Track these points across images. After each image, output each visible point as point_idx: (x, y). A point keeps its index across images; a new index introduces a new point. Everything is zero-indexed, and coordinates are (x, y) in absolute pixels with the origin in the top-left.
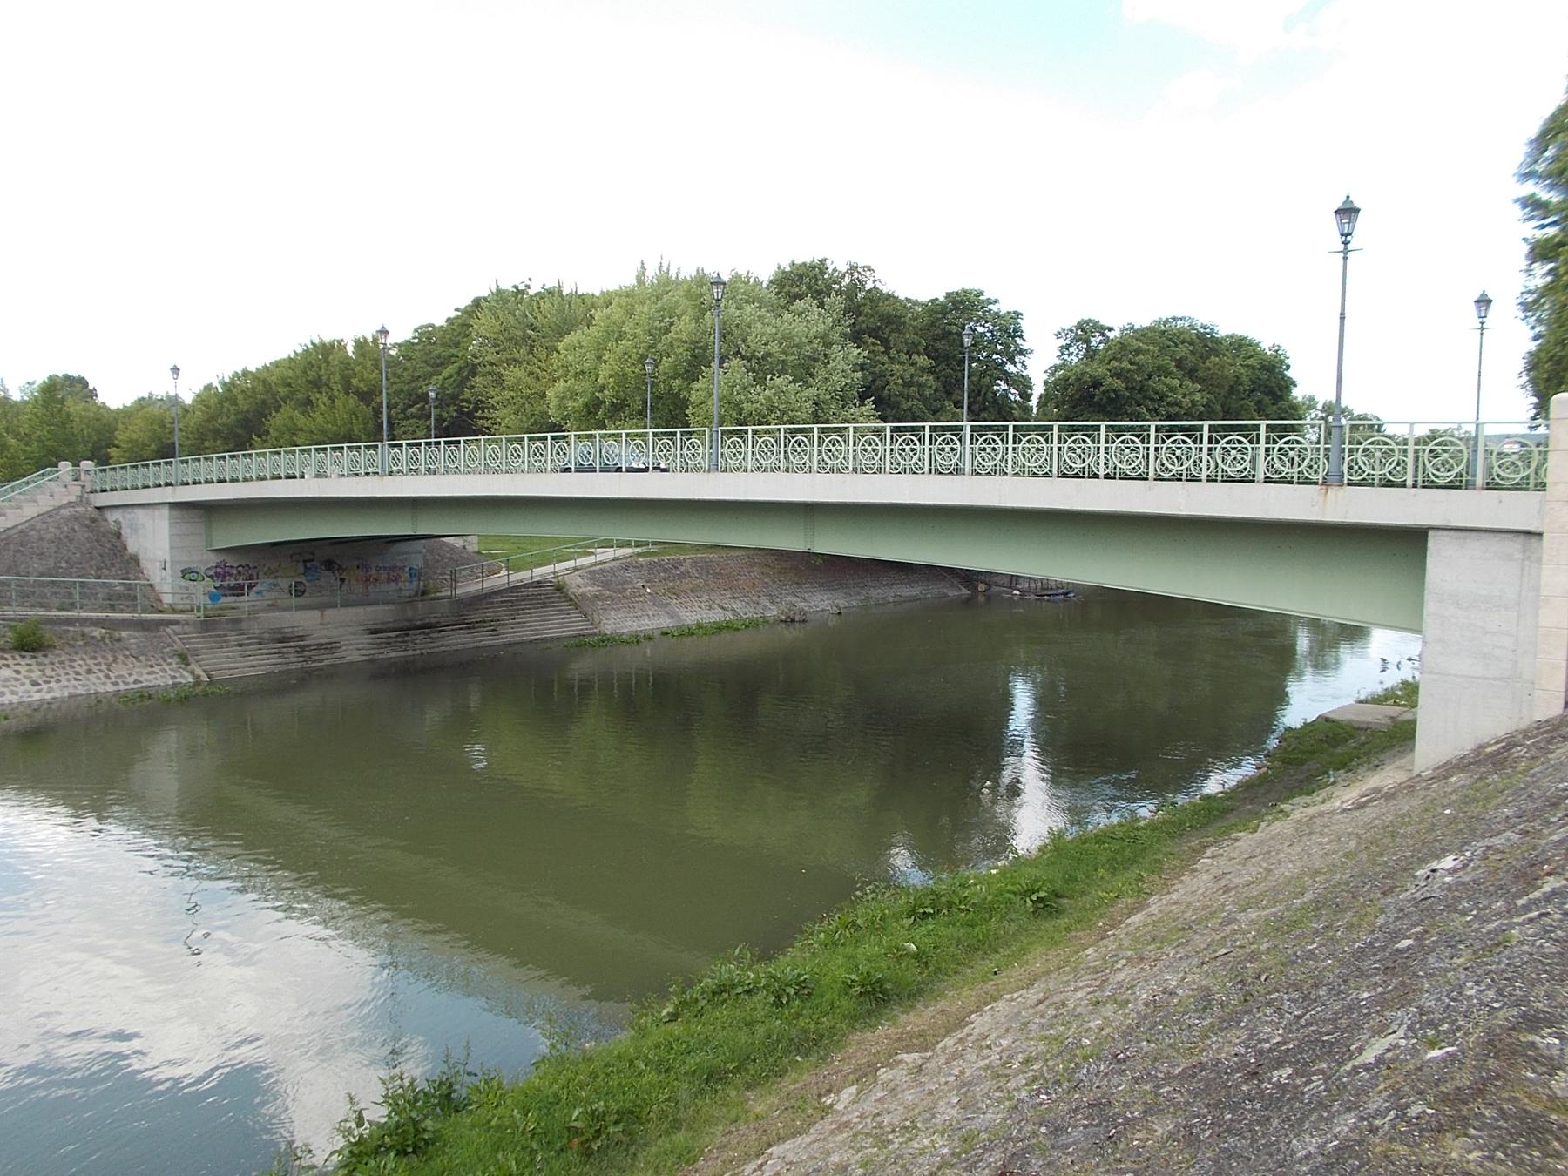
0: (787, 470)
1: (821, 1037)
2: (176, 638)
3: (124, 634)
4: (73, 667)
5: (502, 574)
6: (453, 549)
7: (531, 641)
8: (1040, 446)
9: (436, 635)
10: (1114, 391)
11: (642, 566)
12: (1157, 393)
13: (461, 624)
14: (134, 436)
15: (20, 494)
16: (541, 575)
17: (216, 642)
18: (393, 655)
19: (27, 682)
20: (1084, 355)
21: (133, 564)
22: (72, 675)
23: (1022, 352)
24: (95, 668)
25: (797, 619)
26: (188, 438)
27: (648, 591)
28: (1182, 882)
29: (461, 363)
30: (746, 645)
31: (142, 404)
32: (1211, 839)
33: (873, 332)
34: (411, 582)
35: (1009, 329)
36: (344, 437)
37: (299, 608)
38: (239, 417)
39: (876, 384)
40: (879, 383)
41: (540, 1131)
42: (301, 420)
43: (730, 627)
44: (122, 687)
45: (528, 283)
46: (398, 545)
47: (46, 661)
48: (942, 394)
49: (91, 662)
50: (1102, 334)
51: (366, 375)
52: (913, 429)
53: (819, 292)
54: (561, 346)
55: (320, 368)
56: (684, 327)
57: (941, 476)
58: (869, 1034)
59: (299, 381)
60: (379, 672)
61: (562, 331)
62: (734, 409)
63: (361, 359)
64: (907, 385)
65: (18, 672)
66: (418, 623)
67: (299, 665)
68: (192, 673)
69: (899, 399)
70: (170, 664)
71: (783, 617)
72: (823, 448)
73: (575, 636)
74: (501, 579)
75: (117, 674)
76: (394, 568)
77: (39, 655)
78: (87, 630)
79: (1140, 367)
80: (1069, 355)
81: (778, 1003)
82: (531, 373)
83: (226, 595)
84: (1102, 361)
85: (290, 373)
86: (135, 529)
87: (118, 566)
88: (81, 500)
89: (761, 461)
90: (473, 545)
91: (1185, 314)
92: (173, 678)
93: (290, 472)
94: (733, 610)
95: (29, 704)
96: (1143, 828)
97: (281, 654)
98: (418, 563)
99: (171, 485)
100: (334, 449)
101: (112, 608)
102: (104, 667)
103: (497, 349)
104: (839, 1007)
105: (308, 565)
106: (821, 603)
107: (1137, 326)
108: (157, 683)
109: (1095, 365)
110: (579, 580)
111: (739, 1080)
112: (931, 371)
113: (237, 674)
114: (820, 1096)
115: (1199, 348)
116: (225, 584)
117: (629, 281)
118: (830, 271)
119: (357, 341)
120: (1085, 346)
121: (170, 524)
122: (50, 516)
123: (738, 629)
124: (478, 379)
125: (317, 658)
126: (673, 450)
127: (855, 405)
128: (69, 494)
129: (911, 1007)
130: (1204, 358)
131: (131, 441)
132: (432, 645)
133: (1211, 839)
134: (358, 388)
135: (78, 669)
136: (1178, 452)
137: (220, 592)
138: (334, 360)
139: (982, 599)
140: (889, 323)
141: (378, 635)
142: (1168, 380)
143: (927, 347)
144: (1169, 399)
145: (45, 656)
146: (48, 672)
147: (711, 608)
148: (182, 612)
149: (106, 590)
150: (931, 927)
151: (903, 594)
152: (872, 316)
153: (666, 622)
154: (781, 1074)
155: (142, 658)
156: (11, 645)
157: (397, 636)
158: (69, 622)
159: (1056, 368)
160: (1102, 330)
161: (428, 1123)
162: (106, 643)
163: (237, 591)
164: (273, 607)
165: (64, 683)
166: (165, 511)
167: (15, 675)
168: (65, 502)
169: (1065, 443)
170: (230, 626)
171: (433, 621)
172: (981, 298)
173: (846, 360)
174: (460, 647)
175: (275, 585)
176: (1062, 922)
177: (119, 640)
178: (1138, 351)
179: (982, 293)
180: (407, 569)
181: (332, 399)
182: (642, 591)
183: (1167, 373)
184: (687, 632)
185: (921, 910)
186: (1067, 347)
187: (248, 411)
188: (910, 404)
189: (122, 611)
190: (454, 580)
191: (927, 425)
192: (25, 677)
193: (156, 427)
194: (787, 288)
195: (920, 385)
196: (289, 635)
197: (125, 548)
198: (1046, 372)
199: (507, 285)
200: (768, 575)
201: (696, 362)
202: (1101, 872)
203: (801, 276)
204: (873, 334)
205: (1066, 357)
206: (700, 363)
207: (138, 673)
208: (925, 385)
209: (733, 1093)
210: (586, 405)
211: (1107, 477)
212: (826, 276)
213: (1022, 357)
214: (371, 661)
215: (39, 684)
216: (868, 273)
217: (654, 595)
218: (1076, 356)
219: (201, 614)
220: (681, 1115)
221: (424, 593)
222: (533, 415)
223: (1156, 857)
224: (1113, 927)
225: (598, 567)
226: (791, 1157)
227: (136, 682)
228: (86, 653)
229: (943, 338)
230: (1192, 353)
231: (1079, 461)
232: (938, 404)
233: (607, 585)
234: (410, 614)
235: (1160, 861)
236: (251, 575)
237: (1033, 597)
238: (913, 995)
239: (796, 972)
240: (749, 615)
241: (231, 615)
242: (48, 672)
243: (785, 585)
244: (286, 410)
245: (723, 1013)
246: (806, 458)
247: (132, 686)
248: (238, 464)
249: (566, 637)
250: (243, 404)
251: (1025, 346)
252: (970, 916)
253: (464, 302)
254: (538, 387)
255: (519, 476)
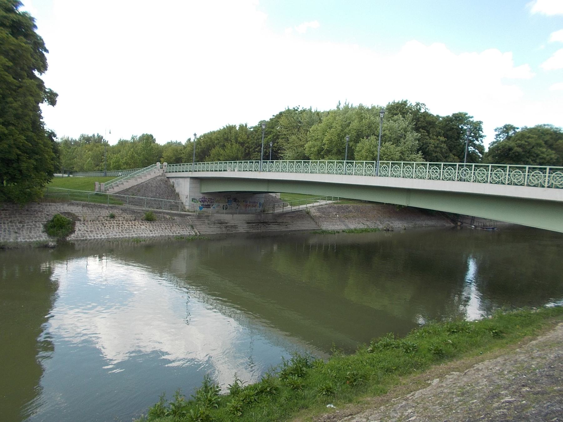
0: (404, 177)
1: (422, 364)
2: (190, 220)
3: (175, 218)
4: (161, 227)
5: (288, 207)
6: (272, 197)
7: (298, 230)
8: (484, 172)
9: (268, 226)
10: (518, 152)
11: (335, 207)
12: (535, 154)
13: (275, 223)
14: (168, 155)
15: (146, 172)
16: (302, 208)
17: (201, 222)
18: (254, 231)
19: (149, 230)
20: (506, 138)
21: (177, 196)
22: (161, 229)
23: (481, 137)
24: (167, 228)
25: (390, 230)
26: (185, 156)
27: (338, 216)
28: (550, 333)
29: (274, 134)
30: (370, 238)
31: (170, 144)
32: (560, 320)
33: (423, 128)
34: (260, 207)
35: (477, 128)
36: (235, 159)
37: (226, 213)
38: (201, 150)
39: (424, 146)
40: (425, 146)
41: (337, 376)
42: (222, 152)
43: (366, 231)
44: (175, 234)
45: (298, 107)
46: (257, 194)
47: (154, 224)
48: (448, 151)
49: (166, 226)
50: (514, 130)
51: (243, 137)
52: (436, 165)
53: (404, 113)
54: (310, 130)
55: (228, 134)
56: (355, 124)
57: (480, 183)
58: (438, 366)
59: (221, 139)
60: (249, 237)
61: (310, 124)
62: (371, 154)
63: (242, 132)
64: (436, 147)
65: (146, 227)
66: (262, 221)
67: (226, 232)
68: (195, 232)
69: (432, 152)
70: (188, 228)
71: (385, 229)
72: (392, 169)
73: (312, 230)
74: (289, 208)
75: (173, 230)
76: (255, 202)
77: (152, 222)
78: (165, 215)
79: (529, 144)
80: (500, 138)
81: (406, 352)
82: (298, 138)
83: (204, 208)
84: (513, 140)
85: (219, 136)
86: (178, 184)
87: (173, 196)
88: (163, 175)
89: (394, 173)
90: (278, 196)
91: (549, 123)
92: (189, 233)
93: (220, 169)
94: (367, 225)
95: (149, 237)
96: (533, 314)
97: (221, 228)
98: (262, 201)
99: (191, 171)
100: (225, 163)
101: (171, 209)
102: (170, 228)
103: (287, 130)
104: (427, 356)
105: (229, 199)
106: (398, 225)
107: (528, 127)
108: (184, 234)
109: (510, 142)
110: (314, 210)
111: (397, 372)
112: (445, 142)
113: (207, 233)
114: (425, 381)
115: (554, 136)
116: (204, 204)
117: (334, 108)
118: (408, 105)
119: (240, 126)
120: (506, 134)
121: (190, 184)
122: (154, 179)
123: (369, 232)
124: (280, 140)
125: (231, 230)
126: (343, 167)
127: (415, 154)
128: (160, 172)
129: (452, 360)
130: (556, 140)
131: (167, 156)
132: (267, 229)
133: (560, 320)
134: (240, 141)
135: (163, 228)
136: (498, 175)
137: (203, 206)
138: (233, 132)
139: (459, 228)
140: (430, 124)
141: (250, 224)
142: (541, 149)
143: (444, 133)
144: (540, 156)
145: (154, 223)
146: (154, 228)
147: (359, 224)
148: (191, 212)
149: (170, 204)
150: (456, 336)
151: (429, 224)
152: (424, 122)
153: (343, 227)
154: (410, 373)
155: (180, 226)
156: (144, 219)
157: (255, 225)
158: (160, 213)
159: (494, 143)
160: (514, 128)
161: (304, 368)
162: (170, 220)
163: (208, 206)
164: (218, 212)
165: (159, 231)
166: (189, 180)
167: (145, 228)
168: (158, 175)
169: (493, 171)
170: (205, 218)
171: (267, 221)
172: (466, 116)
173: (412, 137)
174: (275, 230)
175: (219, 205)
176: (504, 341)
177: (174, 219)
178: (529, 137)
179: (467, 114)
180: (259, 203)
181: (232, 145)
182: (335, 216)
183: (540, 146)
184: (351, 231)
185: (452, 330)
186: (499, 135)
187: (205, 148)
188: (436, 154)
189: (174, 210)
190: (274, 208)
191: (442, 163)
192: (148, 229)
193: (175, 152)
194: (392, 111)
195: (441, 147)
196: (223, 222)
197: (175, 191)
198: (489, 144)
199: (291, 108)
200: (379, 214)
201: (359, 137)
202: (518, 327)
203: (397, 107)
204: (423, 128)
205: (498, 139)
206: (360, 137)
207: (179, 230)
208: (443, 148)
209: (395, 376)
210: (318, 150)
211: (548, 187)
212: (406, 107)
213: (481, 139)
214: (247, 232)
215: (152, 231)
216: (424, 106)
217: (340, 218)
218: (502, 138)
219: (198, 213)
220: (379, 380)
221: (264, 211)
222: (298, 153)
223: (539, 324)
224: (524, 345)
225: (320, 207)
226: (423, 393)
227: (179, 233)
228: (165, 223)
229: (450, 130)
230: (551, 138)
231: (536, 180)
232: (447, 155)
233: (324, 213)
234: (259, 218)
235: (540, 325)
236: (212, 202)
237: (480, 229)
238: (452, 357)
239: (412, 343)
240: (373, 227)
241: (206, 214)
242: (154, 228)
243: (385, 217)
244: (217, 148)
245: (388, 352)
246: (386, 172)
247: (178, 234)
248: (201, 166)
249: (310, 230)
250: (203, 146)
251: (483, 134)
252: (470, 334)
253: (277, 113)
254: (302, 143)
255: (315, 174)
